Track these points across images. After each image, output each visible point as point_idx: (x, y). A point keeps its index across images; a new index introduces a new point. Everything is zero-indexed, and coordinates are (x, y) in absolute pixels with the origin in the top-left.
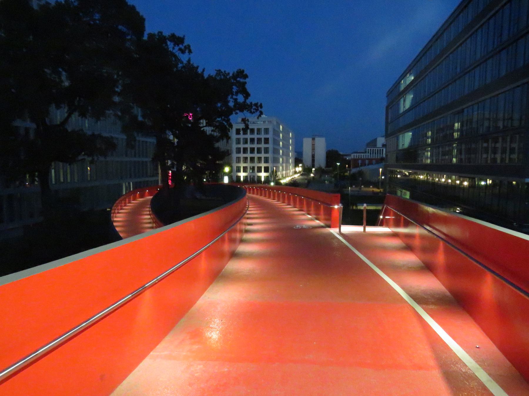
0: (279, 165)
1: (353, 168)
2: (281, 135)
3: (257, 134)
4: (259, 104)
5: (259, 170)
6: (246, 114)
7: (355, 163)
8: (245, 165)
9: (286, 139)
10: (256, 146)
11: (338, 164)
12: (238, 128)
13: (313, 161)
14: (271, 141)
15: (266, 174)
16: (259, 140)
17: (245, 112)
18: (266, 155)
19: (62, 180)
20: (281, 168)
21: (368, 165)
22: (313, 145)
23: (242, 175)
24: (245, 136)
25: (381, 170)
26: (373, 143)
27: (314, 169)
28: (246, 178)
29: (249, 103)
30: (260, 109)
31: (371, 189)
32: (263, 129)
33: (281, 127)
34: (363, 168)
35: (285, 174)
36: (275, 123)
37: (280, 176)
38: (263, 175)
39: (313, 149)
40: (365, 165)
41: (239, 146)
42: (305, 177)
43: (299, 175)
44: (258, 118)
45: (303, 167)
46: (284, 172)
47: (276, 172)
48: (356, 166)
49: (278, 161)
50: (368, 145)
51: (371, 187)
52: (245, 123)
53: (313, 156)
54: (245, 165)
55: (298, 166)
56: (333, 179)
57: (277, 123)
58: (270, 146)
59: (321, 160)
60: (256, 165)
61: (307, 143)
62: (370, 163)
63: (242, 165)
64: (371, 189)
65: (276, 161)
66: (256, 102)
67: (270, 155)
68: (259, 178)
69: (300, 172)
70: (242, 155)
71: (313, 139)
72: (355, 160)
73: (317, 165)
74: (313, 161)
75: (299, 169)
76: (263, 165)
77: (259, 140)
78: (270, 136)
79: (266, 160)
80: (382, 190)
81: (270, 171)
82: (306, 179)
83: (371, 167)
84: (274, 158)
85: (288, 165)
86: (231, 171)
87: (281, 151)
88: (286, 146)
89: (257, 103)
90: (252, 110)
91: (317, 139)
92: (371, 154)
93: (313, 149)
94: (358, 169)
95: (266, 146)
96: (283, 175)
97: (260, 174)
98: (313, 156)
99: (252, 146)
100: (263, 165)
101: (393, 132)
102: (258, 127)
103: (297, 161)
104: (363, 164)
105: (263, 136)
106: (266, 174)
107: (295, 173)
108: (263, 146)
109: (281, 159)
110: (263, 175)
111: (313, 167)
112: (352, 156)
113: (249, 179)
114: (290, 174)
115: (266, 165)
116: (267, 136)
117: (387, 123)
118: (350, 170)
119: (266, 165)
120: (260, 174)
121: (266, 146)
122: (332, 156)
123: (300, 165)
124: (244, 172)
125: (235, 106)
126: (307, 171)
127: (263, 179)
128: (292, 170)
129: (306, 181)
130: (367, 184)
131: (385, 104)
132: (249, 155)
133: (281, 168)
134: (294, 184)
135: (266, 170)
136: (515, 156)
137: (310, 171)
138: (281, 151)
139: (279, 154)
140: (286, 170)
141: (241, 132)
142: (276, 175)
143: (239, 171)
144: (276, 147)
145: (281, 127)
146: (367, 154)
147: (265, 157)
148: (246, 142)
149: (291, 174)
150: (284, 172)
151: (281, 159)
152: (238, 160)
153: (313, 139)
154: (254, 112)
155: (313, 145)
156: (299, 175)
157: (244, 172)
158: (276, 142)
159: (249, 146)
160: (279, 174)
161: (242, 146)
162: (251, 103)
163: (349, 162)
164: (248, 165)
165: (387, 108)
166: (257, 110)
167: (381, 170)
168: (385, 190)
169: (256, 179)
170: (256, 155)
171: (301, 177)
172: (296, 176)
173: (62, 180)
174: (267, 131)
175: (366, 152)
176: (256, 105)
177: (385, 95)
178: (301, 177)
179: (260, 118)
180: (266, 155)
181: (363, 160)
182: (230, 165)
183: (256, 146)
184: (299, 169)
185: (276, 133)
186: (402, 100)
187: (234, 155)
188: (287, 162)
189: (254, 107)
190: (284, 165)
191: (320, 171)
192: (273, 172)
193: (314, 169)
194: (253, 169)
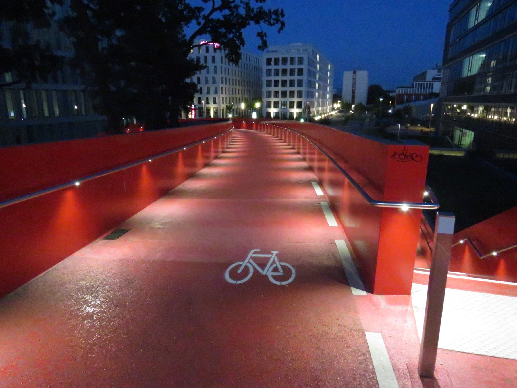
0: (314, 100)
1: (397, 104)
2: (318, 66)
3: (290, 64)
4: (280, 11)
5: (292, 106)
6: (263, 26)
7: (400, 99)
8: (276, 100)
9: (323, 70)
10: (288, 78)
11: (381, 99)
12: (269, 57)
13: (353, 97)
14: (305, 72)
15: (276, 110)
16: (292, 72)
17: (261, 22)
18: (300, 89)
19: (47, 114)
20: (316, 103)
21: (415, 101)
22: (354, 79)
23: (273, 111)
24: (277, 67)
25: (432, 105)
26: (422, 76)
27: (353, 106)
28: (277, 114)
29: (267, 11)
30: (280, 18)
31: (419, 128)
32: (297, 59)
33: (318, 57)
34: (412, 104)
35: (321, 110)
36: (311, 52)
37: (316, 113)
38: (295, 111)
39: (354, 84)
40: (411, 101)
41: (269, 78)
42: (343, 114)
43: (337, 111)
44: (279, 32)
45: (342, 103)
46: (320, 108)
47: (310, 108)
48: (401, 102)
49: (313, 96)
50: (416, 79)
51: (419, 125)
52: (262, 39)
53: (353, 92)
54: (276, 100)
55: (337, 103)
56: (375, 116)
57: (313, 51)
58: (304, 77)
59: (362, 96)
60: (288, 99)
61: (348, 76)
62: (417, 99)
63: (273, 100)
64: (419, 128)
65: (310, 95)
66: (276, 8)
67: (304, 89)
68: (292, 114)
69: (338, 109)
70: (273, 89)
71: (355, 73)
72: (400, 96)
73: (357, 100)
74: (353, 97)
75: (337, 105)
76: (296, 100)
77: (292, 72)
78: (304, 66)
79: (300, 95)
80: (433, 129)
81: (303, 106)
82: (343, 116)
83: (418, 103)
84: (308, 92)
85: (325, 100)
86: (261, 108)
87: (317, 85)
88: (323, 79)
89: (277, 11)
90: (272, 21)
91: (358, 73)
92: (418, 89)
93: (354, 84)
94: (404, 105)
95: (300, 78)
96: (318, 111)
97: (270, 110)
98: (353, 92)
99: (285, 78)
100: (296, 100)
101: (453, 57)
102: (292, 56)
103: (335, 98)
104: (409, 101)
105: (296, 67)
106: (276, 110)
107: (333, 109)
108: (296, 78)
109: (317, 94)
110: (295, 111)
111: (353, 103)
112: (397, 92)
113: (280, 116)
114: (328, 109)
115: (299, 100)
116: (301, 67)
117: (447, 46)
118: (394, 107)
119: (299, 100)
120: (270, 110)
121: (300, 78)
122: (374, 91)
123: (339, 101)
124: (275, 107)
125: (247, 14)
126: (346, 107)
127: (295, 116)
128: (329, 107)
129: (343, 118)
130: (414, 122)
131: (446, 22)
132: (280, 89)
133: (316, 103)
134: (326, 122)
135: (300, 105)
136: (334, 113)
137: (350, 108)
138: (317, 85)
139: (315, 87)
140: (323, 105)
141: (273, 63)
142: (310, 111)
143: (269, 106)
144: (311, 79)
145: (318, 57)
146: (414, 89)
147: (298, 91)
148: (277, 73)
149: (328, 110)
150: (320, 108)
151: (317, 94)
152: (269, 95)
153: (355, 73)
154: (274, 24)
155: (354, 79)
156: (337, 111)
157: (297, 108)
158: (312, 74)
159: (280, 78)
160: (314, 110)
161: (273, 78)
162: (270, 11)
163: (392, 99)
164: (279, 99)
165: (449, 26)
166: (277, 21)
167: (432, 105)
168: (437, 129)
169: (288, 116)
170: (288, 89)
171: (339, 114)
172: (334, 113)
173: (47, 114)
174: (301, 61)
175: (413, 87)
176: (276, 12)
177: (448, 9)
178: (339, 114)
179: (281, 31)
180: (300, 89)
181: (410, 96)
182: (260, 100)
183: (288, 78)
184: (337, 105)
185: (312, 63)
186: (474, 10)
187: (265, 89)
188: (324, 97)
189: (274, 16)
190: (320, 100)
191: (360, 108)
192: (306, 107)
193: (353, 106)
194: (284, 104)
